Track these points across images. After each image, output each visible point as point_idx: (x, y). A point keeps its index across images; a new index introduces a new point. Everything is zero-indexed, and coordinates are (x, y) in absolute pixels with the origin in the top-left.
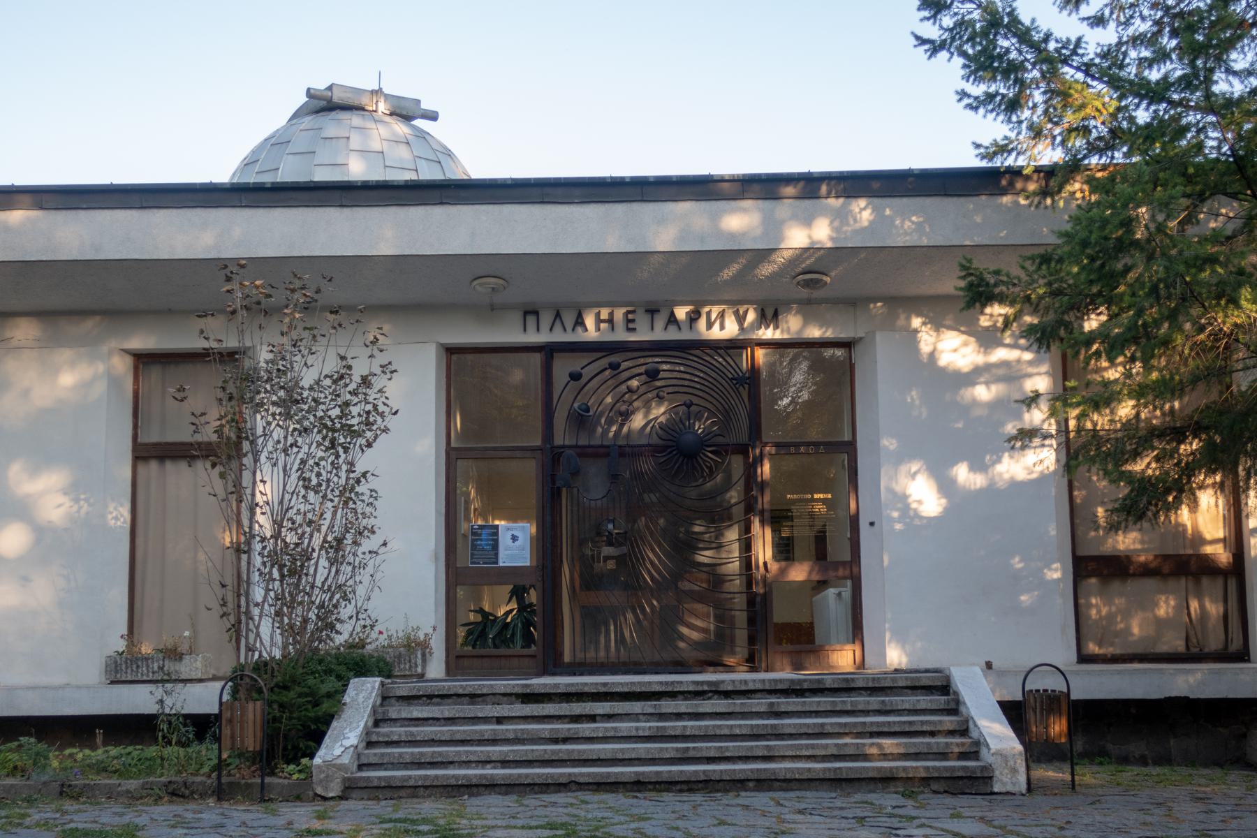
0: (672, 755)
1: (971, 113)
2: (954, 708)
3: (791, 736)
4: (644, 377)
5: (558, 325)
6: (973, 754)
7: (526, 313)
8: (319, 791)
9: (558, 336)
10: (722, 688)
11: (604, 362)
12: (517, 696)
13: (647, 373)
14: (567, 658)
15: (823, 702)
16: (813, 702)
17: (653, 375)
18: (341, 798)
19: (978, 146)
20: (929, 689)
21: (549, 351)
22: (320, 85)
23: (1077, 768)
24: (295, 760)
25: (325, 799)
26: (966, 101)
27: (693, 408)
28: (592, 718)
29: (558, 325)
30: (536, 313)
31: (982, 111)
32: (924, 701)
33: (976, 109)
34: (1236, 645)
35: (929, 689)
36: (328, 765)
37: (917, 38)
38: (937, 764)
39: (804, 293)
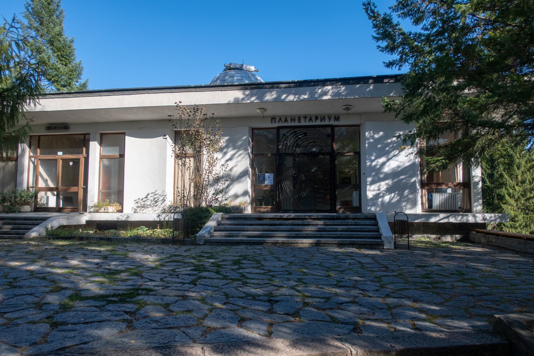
0: (294, 235)
1: (382, 53)
2: (376, 224)
3: (328, 231)
4: (303, 135)
5: (280, 122)
6: (380, 238)
7: (272, 119)
8: (198, 242)
9: (281, 124)
10: (312, 217)
11: (292, 131)
12: (257, 218)
13: (304, 134)
14: (282, 209)
15: (339, 222)
16: (336, 222)
17: (305, 134)
18: (204, 245)
19: (384, 63)
20: (370, 219)
21: (279, 128)
22: (228, 64)
23: (407, 243)
24: (193, 234)
25: (199, 245)
26: (380, 49)
27: (316, 143)
28: (275, 225)
29: (280, 122)
30: (275, 118)
31: (385, 52)
32: (368, 222)
33: (383, 51)
34: (468, 208)
35: (370, 219)
36: (200, 236)
37: (373, 37)
38: (368, 240)
39: (346, 112)
